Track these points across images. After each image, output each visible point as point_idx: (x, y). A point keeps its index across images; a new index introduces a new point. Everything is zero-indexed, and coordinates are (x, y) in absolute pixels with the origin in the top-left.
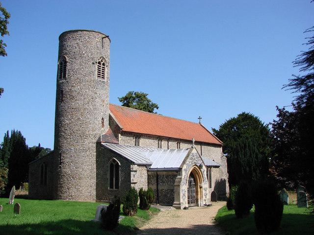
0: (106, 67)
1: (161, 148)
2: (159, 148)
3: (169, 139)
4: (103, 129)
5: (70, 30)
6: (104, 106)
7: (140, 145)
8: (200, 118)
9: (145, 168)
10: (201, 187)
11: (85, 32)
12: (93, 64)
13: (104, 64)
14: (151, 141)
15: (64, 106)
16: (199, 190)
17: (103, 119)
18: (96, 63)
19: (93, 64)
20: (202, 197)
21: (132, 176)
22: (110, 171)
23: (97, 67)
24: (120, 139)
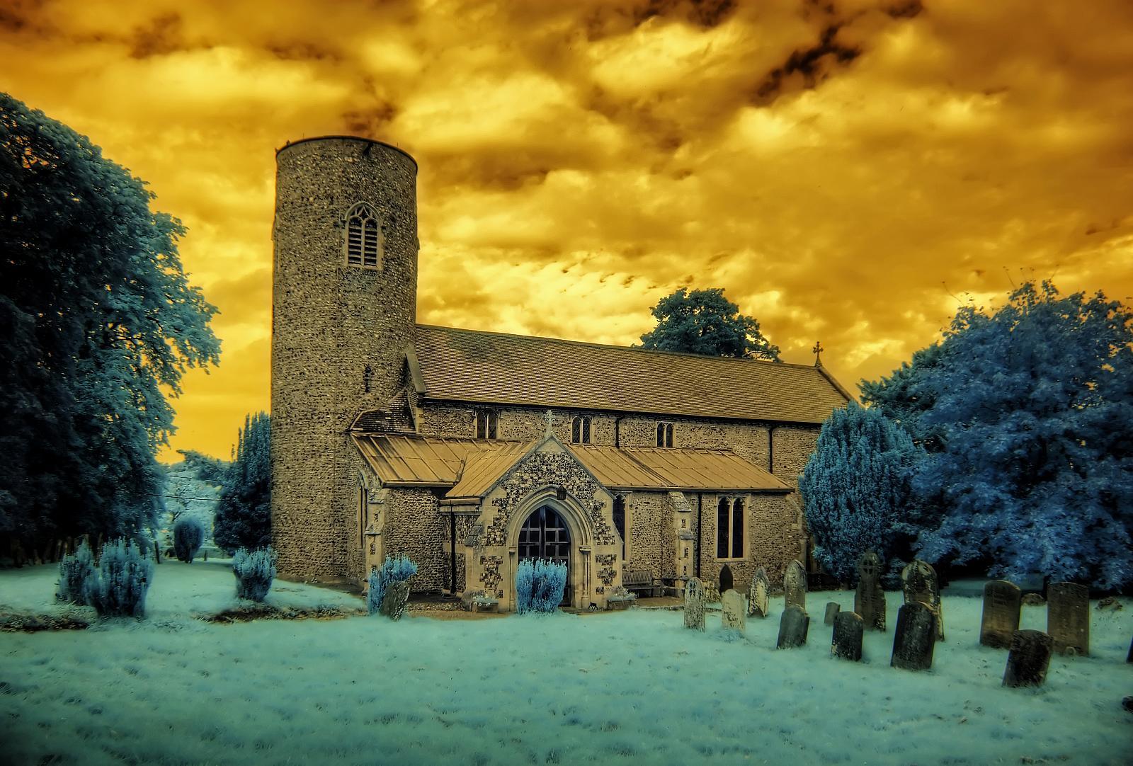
0: (379, 230)
1: (670, 444)
2: (660, 444)
4: (368, 396)
7: (499, 436)
12: (336, 225)
17: (368, 370)
18: (344, 222)
19: (336, 225)
20: (589, 581)
24: (418, 421)
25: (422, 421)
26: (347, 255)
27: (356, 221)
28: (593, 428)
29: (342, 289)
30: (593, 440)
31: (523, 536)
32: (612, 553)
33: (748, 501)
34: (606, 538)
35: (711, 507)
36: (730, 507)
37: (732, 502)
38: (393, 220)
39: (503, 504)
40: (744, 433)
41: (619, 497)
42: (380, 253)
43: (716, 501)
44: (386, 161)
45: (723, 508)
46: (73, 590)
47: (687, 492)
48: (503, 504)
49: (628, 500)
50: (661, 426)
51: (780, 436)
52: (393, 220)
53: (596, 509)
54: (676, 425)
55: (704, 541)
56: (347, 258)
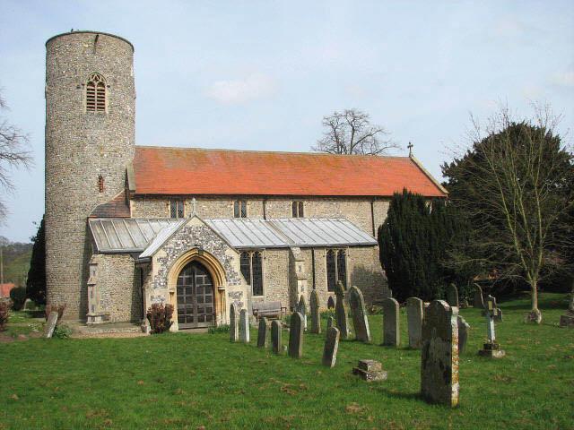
0: (106, 89)
2: (295, 215)
3: (265, 198)
4: (100, 195)
5: (55, 35)
6: (102, 155)
8: (410, 147)
9: (127, 258)
10: (221, 291)
11: (64, 38)
12: (78, 88)
13: (101, 84)
14: (217, 204)
15: (60, 158)
16: (218, 295)
17: (101, 178)
21: (91, 273)
22: (261, 273)
23: (85, 92)
24: (132, 209)
25: (134, 208)
26: (86, 105)
27: (91, 84)
28: (248, 207)
29: (83, 127)
30: (305, 215)
31: (179, 281)
32: (240, 290)
33: (348, 251)
34: (235, 281)
35: (321, 258)
36: (336, 257)
37: (336, 252)
38: (115, 81)
39: (164, 261)
40: (353, 205)
41: (331, 251)
42: (107, 103)
43: (325, 252)
44: (109, 44)
45: (330, 257)
46: (461, 380)
47: (303, 248)
48: (164, 261)
49: (264, 254)
50: (294, 203)
51: (270, 205)
52: (115, 81)
53: (227, 261)
54: (305, 203)
55: (317, 280)
56: (85, 108)
